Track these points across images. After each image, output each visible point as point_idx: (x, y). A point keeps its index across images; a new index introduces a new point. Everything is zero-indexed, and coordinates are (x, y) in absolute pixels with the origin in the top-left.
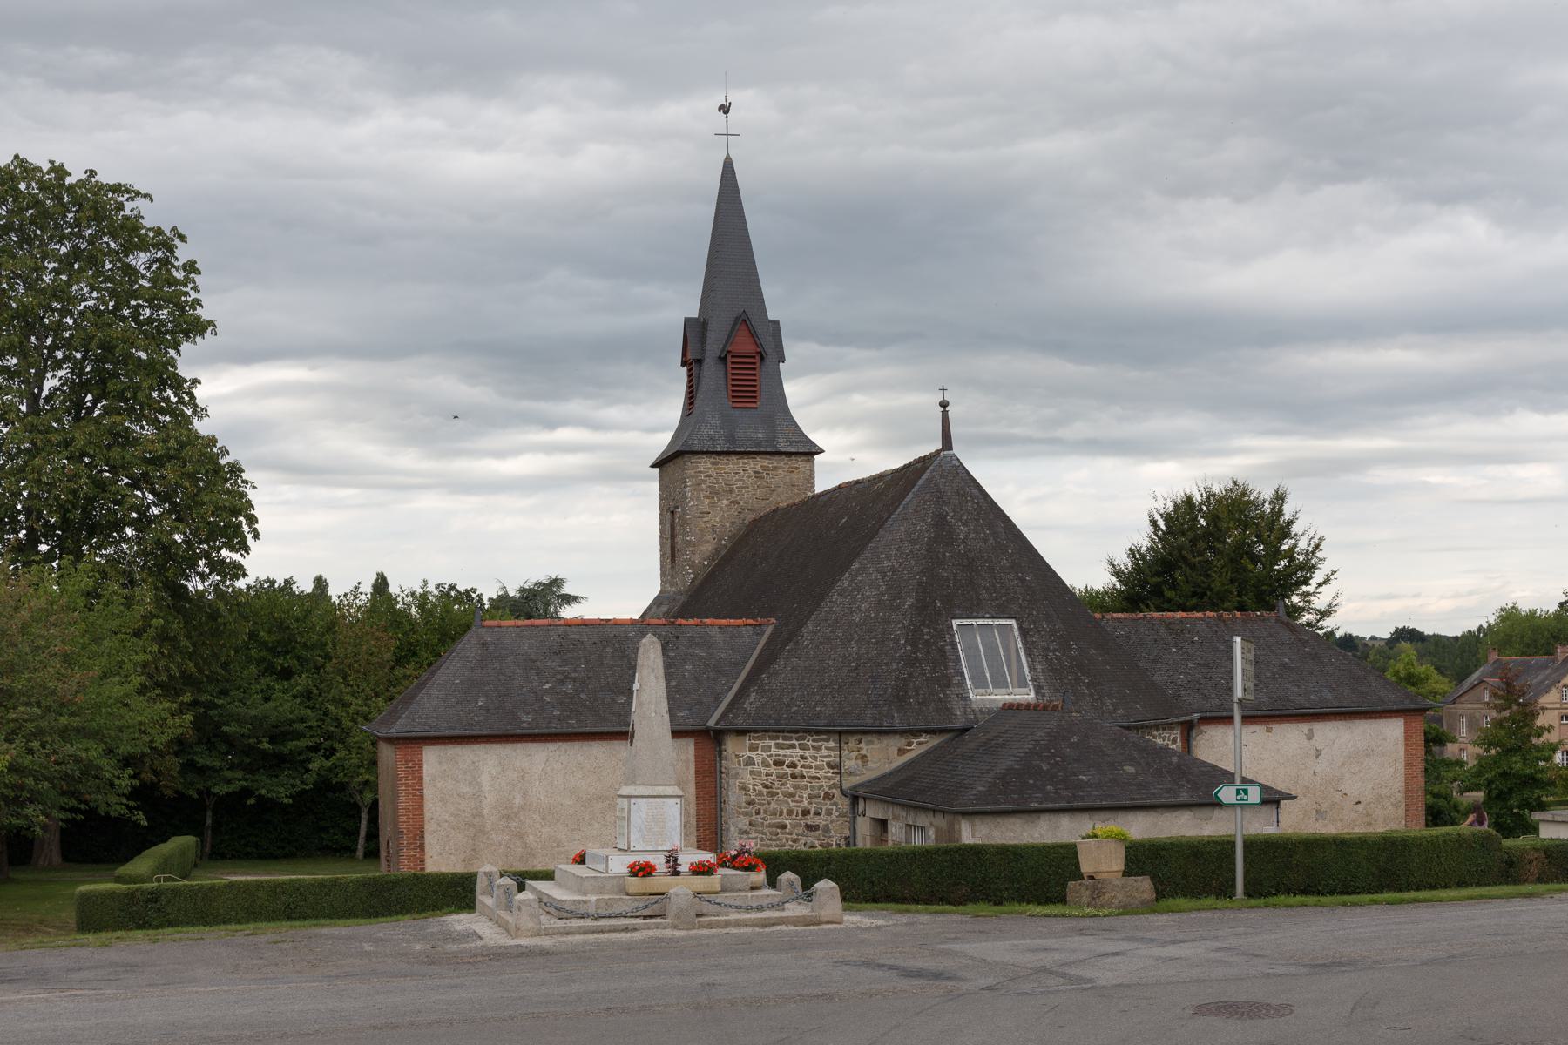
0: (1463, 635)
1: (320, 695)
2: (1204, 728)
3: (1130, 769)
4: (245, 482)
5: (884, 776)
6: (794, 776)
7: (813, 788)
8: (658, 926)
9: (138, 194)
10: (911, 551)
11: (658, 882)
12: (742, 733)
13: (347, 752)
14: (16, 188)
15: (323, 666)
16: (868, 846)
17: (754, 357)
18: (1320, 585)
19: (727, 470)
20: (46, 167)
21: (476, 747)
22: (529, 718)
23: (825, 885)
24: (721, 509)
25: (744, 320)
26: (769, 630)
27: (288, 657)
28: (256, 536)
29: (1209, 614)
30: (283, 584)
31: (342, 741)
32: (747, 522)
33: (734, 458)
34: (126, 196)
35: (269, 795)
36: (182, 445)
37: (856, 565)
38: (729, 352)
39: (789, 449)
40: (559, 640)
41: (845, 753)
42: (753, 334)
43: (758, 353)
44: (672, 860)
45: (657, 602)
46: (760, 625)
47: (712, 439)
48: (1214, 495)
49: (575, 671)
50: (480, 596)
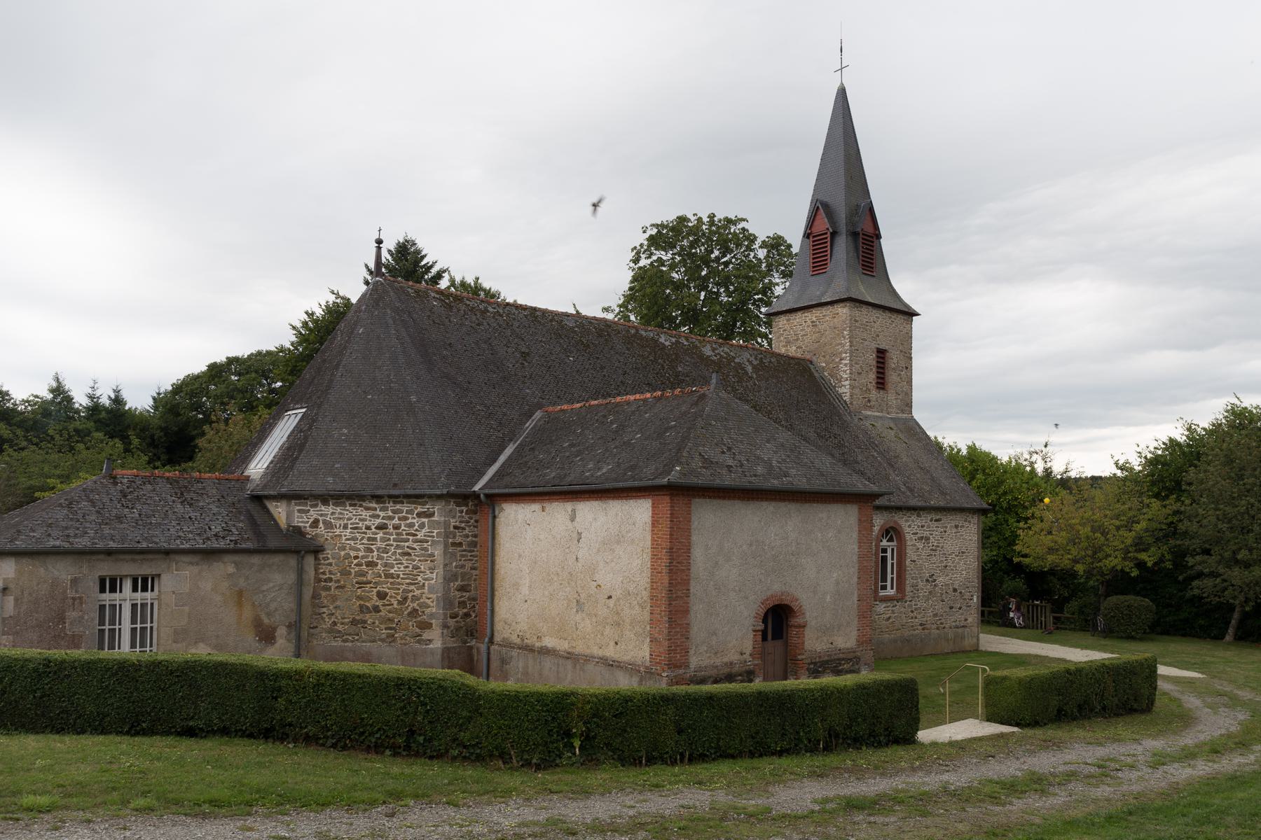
0: (250, 356)
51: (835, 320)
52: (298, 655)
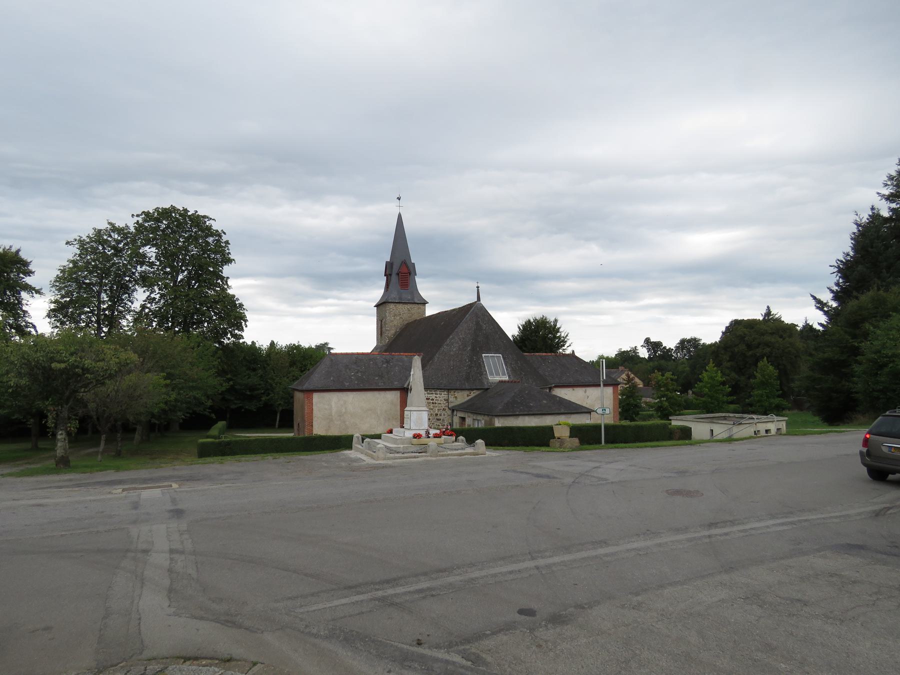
2: (554, 389)
3: (545, 402)
4: (244, 309)
5: (463, 404)
6: (433, 403)
8: (425, 456)
9: (211, 219)
11: (424, 440)
14: (171, 215)
16: (458, 427)
18: (568, 347)
20: (181, 209)
22: (348, 384)
23: (480, 442)
28: (246, 326)
29: (553, 354)
31: (272, 391)
33: (401, 304)
34: (207, 219)
36: (224, 297)
37: (451, 337)
39: (418, 302)
42: (407, 267)
44: (428, 433)
45: (376, 348)
48: (537, 320)
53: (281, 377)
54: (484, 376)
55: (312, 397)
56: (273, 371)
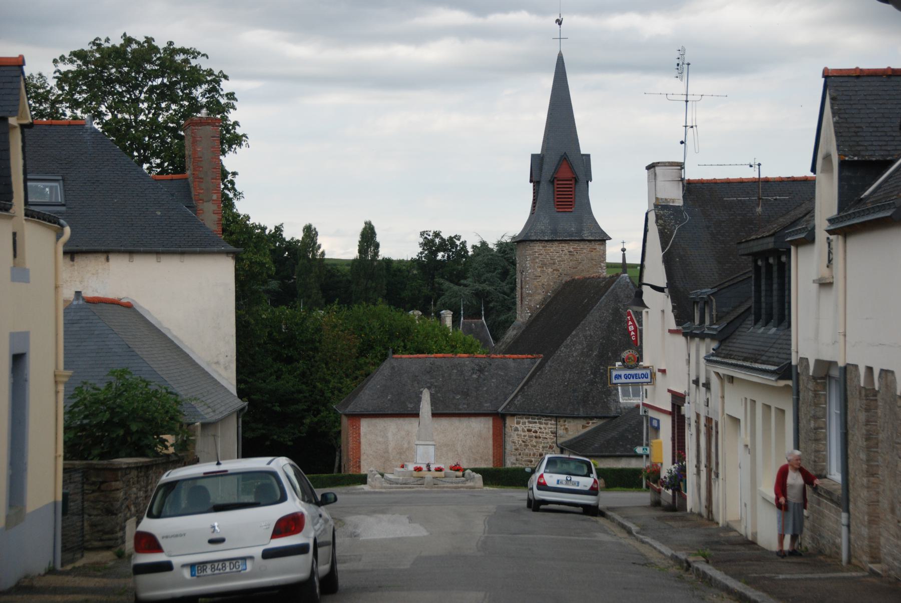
1: (311, 375)
6: (536, 437)
7: (544, 443)
8: (420, 487)
10: (600, 327)
12: (513, 415)
13: (328, 412)
15: (314, 357)
17: (571, 180)
19: (552, 250)
21: (386, 419)
24: (548, 274)
25: (565, 158)
26: (539, 361)
27: (291, 349)
30: (273, 231)
32: (563, 282)
33: (556, 244)
35: (279, 439)
37: (574, 333)
38: (555, 178)
39: (590, 238)
40: (430, 365)
41: (559, 426)
42: (571, 167)
43: (573, 178)
44: (428, 466)
46: (535, 358)
47: (543, 233)
49: (436, 382)
50: (464, 243)
51: (592, 253)
52: (417, 415)
53: (341, 378)
54: (613, 397)
55: (360, 425)
56: (327, 364)
